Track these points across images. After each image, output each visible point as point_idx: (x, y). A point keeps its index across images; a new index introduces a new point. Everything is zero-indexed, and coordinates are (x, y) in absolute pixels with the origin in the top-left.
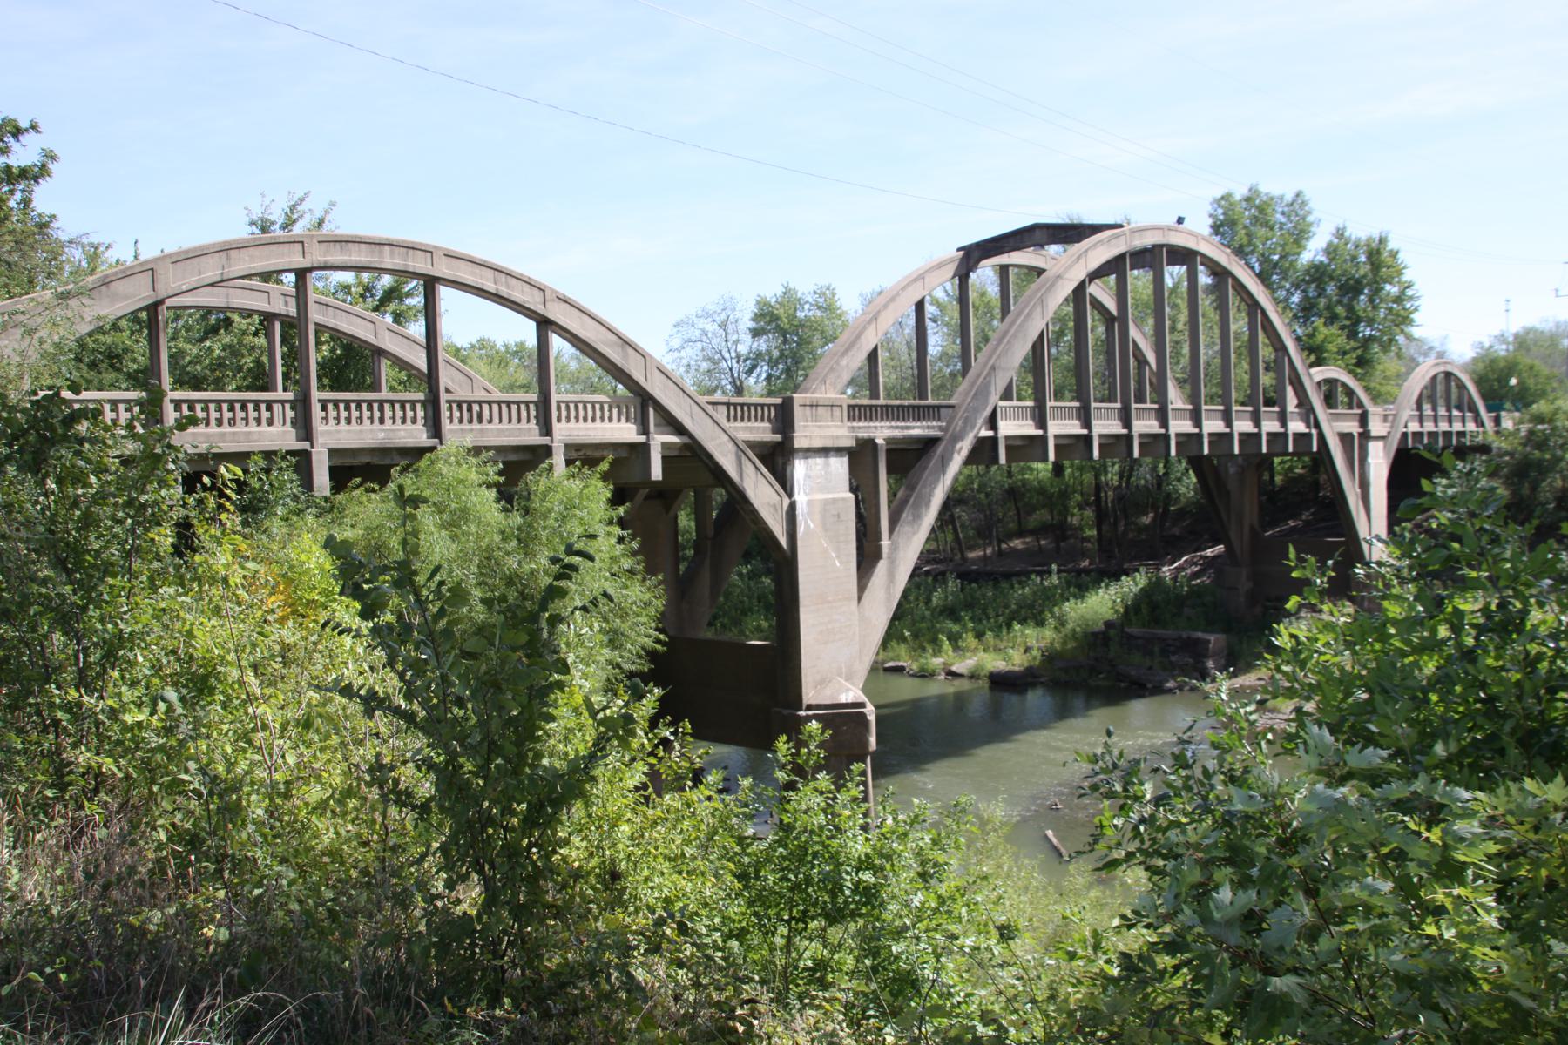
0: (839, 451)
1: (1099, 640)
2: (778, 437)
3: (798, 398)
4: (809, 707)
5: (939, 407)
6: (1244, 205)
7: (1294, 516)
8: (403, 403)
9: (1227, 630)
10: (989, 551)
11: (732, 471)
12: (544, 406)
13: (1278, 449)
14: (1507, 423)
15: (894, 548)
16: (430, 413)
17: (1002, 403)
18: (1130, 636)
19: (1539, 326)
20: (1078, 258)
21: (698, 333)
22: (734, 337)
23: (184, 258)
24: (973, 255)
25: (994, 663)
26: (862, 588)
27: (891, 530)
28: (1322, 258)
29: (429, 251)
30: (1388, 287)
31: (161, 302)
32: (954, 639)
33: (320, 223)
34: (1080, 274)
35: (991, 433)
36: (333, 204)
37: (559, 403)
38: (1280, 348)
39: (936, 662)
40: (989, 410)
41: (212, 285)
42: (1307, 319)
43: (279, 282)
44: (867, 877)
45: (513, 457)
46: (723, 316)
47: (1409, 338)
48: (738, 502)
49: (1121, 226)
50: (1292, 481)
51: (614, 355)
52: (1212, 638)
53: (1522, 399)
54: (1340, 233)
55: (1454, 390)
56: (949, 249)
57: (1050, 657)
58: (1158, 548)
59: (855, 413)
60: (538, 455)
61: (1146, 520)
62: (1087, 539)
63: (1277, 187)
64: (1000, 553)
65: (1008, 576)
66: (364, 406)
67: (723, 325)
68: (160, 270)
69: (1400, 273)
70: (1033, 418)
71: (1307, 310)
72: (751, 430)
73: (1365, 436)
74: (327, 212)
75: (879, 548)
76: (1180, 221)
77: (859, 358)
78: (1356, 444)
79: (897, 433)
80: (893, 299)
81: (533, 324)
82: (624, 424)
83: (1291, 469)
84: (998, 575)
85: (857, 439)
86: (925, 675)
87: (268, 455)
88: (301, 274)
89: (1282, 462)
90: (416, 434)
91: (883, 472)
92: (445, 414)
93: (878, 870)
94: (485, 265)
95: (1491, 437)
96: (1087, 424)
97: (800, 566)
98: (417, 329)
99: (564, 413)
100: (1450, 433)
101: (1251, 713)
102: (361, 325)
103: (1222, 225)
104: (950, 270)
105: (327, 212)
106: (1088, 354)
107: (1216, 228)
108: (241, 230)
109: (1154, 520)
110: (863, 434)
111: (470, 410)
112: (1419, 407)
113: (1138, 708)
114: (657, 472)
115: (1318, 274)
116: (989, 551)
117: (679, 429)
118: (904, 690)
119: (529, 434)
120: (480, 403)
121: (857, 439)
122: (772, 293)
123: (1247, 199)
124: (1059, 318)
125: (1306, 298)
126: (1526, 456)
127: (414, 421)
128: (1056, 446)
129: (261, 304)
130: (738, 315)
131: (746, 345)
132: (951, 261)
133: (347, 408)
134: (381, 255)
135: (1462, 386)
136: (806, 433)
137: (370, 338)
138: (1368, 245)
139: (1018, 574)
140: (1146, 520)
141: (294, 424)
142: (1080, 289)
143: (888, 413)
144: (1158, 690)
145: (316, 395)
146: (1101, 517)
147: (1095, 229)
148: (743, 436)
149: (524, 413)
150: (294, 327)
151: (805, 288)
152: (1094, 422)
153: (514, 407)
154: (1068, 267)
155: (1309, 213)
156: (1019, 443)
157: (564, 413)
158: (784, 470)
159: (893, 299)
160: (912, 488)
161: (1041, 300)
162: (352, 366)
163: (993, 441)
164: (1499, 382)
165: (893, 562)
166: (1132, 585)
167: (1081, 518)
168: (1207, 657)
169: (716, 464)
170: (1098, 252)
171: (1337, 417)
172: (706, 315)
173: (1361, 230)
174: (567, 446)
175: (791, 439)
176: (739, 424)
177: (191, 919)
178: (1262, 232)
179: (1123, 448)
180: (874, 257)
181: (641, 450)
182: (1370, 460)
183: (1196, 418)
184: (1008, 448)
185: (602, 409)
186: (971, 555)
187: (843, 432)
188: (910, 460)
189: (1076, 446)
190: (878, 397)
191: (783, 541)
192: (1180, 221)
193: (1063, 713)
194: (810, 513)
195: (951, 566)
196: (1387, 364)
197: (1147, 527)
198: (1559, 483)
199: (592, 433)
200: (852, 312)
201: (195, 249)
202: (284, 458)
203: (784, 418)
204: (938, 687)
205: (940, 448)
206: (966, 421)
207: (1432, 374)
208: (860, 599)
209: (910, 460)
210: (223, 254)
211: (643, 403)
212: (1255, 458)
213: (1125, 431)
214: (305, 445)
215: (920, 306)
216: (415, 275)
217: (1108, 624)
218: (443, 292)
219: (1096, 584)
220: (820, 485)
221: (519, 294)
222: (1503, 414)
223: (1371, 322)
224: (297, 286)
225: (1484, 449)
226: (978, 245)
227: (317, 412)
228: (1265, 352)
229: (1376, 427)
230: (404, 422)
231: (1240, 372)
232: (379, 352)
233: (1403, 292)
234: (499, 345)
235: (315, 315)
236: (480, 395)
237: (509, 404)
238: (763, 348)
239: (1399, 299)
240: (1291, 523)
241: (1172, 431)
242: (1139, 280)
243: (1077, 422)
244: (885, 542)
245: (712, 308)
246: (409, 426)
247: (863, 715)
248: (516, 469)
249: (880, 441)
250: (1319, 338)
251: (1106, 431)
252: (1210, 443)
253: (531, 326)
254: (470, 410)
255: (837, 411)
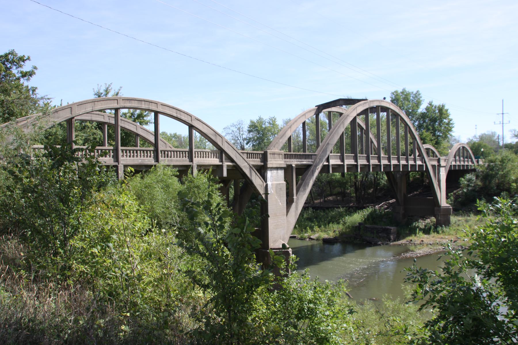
0: (281, 168)
1: (357, 228)
2: (262, 164)
3: (269, 151)
4: (271, 249)
5: (312, 155)
6: (401, 94)
7: (417, 191)
8: (143, 151)
9: (397, 226)
10: (322, 200)
11: (249, 175)
12: (190, 152)
13: (414, 169)
14: (481, 163)
15: (298, 199)
16: (155, 154)
17: (331, 154)
18: (367, 227)
19: (486, 133)
20: (354, 110)
21: (231, 131)
22: (242, 133)
23: (80, 104)
24: (320, 108)
25: (324, 235)
26: (288, 212)
27: (297, 194)
28: (425, 111)
29: (156, 103)
30: (445, 120)
31: (73, 118)
32: (312, 228)
33: (117, 94)
34: (354, 114)
35: (327, 163)
36: (121, 87)
37: (195, 152)
38: (414, 138)
39: (306, 235)
40: (327, 156)
41: (87, 113)
42: (420, 129)
43: (105, 112)
44: (311, 305)
45: (181, 169)
46: (239, 126)
47: (451, 135)
48: (249, 183)
49: (366, 100)
50: (415, 179)
51: (213, 138)
52: (392, 228)
53: (484, 155)
54: (430, 104)
55: (465, 152)
56: (313, 106)
57: (342, 234)
58: (375, 200)
59: (286, 156)
60: (187, 167)
61: (371, 191)
62: (352, 197)
63: (411, 89)
64: (325, 201)
65: (328, 208)
66: (128, 151)
67: (239, 129)
68: (73, 108)
69: (448, 116)
70: (340, 159)
71: (420, 127)
72: (254, 161)
73: (439, 166)
74: (119, 90)
75: (293, 199)
76: (384, 98)
77: (286, 139)
78: (437, 168)
79: (299, 163)
80: (296, 121)
81: (188, 127)
82: (215, 159)
83: (415, 176)
84: (325, 208)
85: (287, 165)
86: (302, 239)
87: (108, 167)
88: (117, 110)
89: (412, 174)
90: (150, 161)
91: (295, 175)
92: (160, 155)
93: (315, 304)
94: (173, 108)
95: (476, 167)
96: (356, 161)
97: (269, 204)
98: (151, 128)
99: (197, 155)
100: (456, 165)
101: (460, 254)
102: (131, 126)
103: (394, 100)
104: (314, 112)
105: (119, 90)
106: (354, 140)
107: (392, 101)
108: (92, 97)
109: (373, 191)
110: (289, 163)
111: (164, 153)
112: (455, 157)
113: (369, 251)
114: (225, 174)
115: (423, 116)
116: (322, 200)
117: (232, 160)
118: (298, 244)
119: (185, 161)
120: (168, 151)
121: (287, 165)
122: (255, 119)
123: (402, 93)
124: (347, 129)
125: (419, 123)
126: (487, 173)
127: (150, 157)
128: (347, 168)
129: (101, 119)
130: (243, 126)
131: (246, 135)
132: (313, 110)
133: (130, 152)
134: (141, 104)
135: (467, 151)
136: (271, 162)
137: (135, 130)
138: (439, 107)
139: (331, 208)
140: (371, 191)
141: (113, 157)
142: (355, 119)
143: (296, 157)
144: (376, 244)
145: (120, 148)
146: (357, 190)
147: (359, 101)
148: (252, 163)
149: (181, 155)
150: (113, 127)
151: (266, 117)
152: (359, 161)
153: (178, 153)
154: (351, 112)
155: (421, 97)
156: (336, 167)
157: (197, 155)
158: (264, 174)
159: (296, 121)
160: (303, 180)
161: (343, 122)
162: (129, 138)
163: (328, 166)
164: (477, 149)
165: (297, 203)
166: (367, 212)
167: (350, 190)
168: (390, 234)
169: (243, 172)
170: (360, 108)
171: (431, 160)
172: (233, 125)
173: (437, 103)
174: (198, 166)
175: (267, 164)
176: (250, 159)
177: (115, 324)
178: (407, 103)
179: (367, 169)
180: (288, 107)
181: (220, 167)
182: (441, 173)
183: (389, 160)
184: (333, 168)
185: (208, 154)
186: (316, 201)
187: (282, 162)
188: (303, 171)
189: (353, 168)
190: (291, 152)
191: (264, 196)
192: (384, 98)
193: (343, 252)
194: (272, 188)
195: (310, 205)
196: (444, 144)
197: (370, 193)
198: (497, 181)
199: (205, 161)
200: (280, 125)
201: (84, 101)
202: (112, 168)
203: (264, 158)
204: (307, 243)
205: (312, 168)
206: (320, 159)
207: (459, 147)
208: (287, 215)
209: (303, 171)
210: (93, 103)
211: (221, 152)
212: (406, 172)
213: (368, 163)
214: (116, 164)
215: (304, 124)
216: (152, 111)
217: (360, 224)
218: (161, 117)
219: (355, 212)
220: (275, 180)
221: (184, 117)
222: (480, 160)
223: (439, 131)
224: (115, 114)
225: (474, 170)
226: (322, 105)
227: (120, 153)
228: (410, 140)
229: (443, 163)
230: (147, 157)
231: (402, 146)
232: (138, 135)
233: (449, 122)
234: (168, 134)
235: (121, 124)
236: (169, 149)
237: (177, 151)
238: (251, 136)
239: (448, 124)
240: (415, 193)
241: (382, 164)
242: (373, 117)
243: (353, 160)
244: (295, 197)
245: (235, 123)
246: (149, 158)
247: (288, 252)
248: (183, 171)
249: (294, 165)
250: (424, 136)
251: (362, 163)
252: (402, 167)
253: (187, 128)
254: (164, 153)
255: (281, 156)
